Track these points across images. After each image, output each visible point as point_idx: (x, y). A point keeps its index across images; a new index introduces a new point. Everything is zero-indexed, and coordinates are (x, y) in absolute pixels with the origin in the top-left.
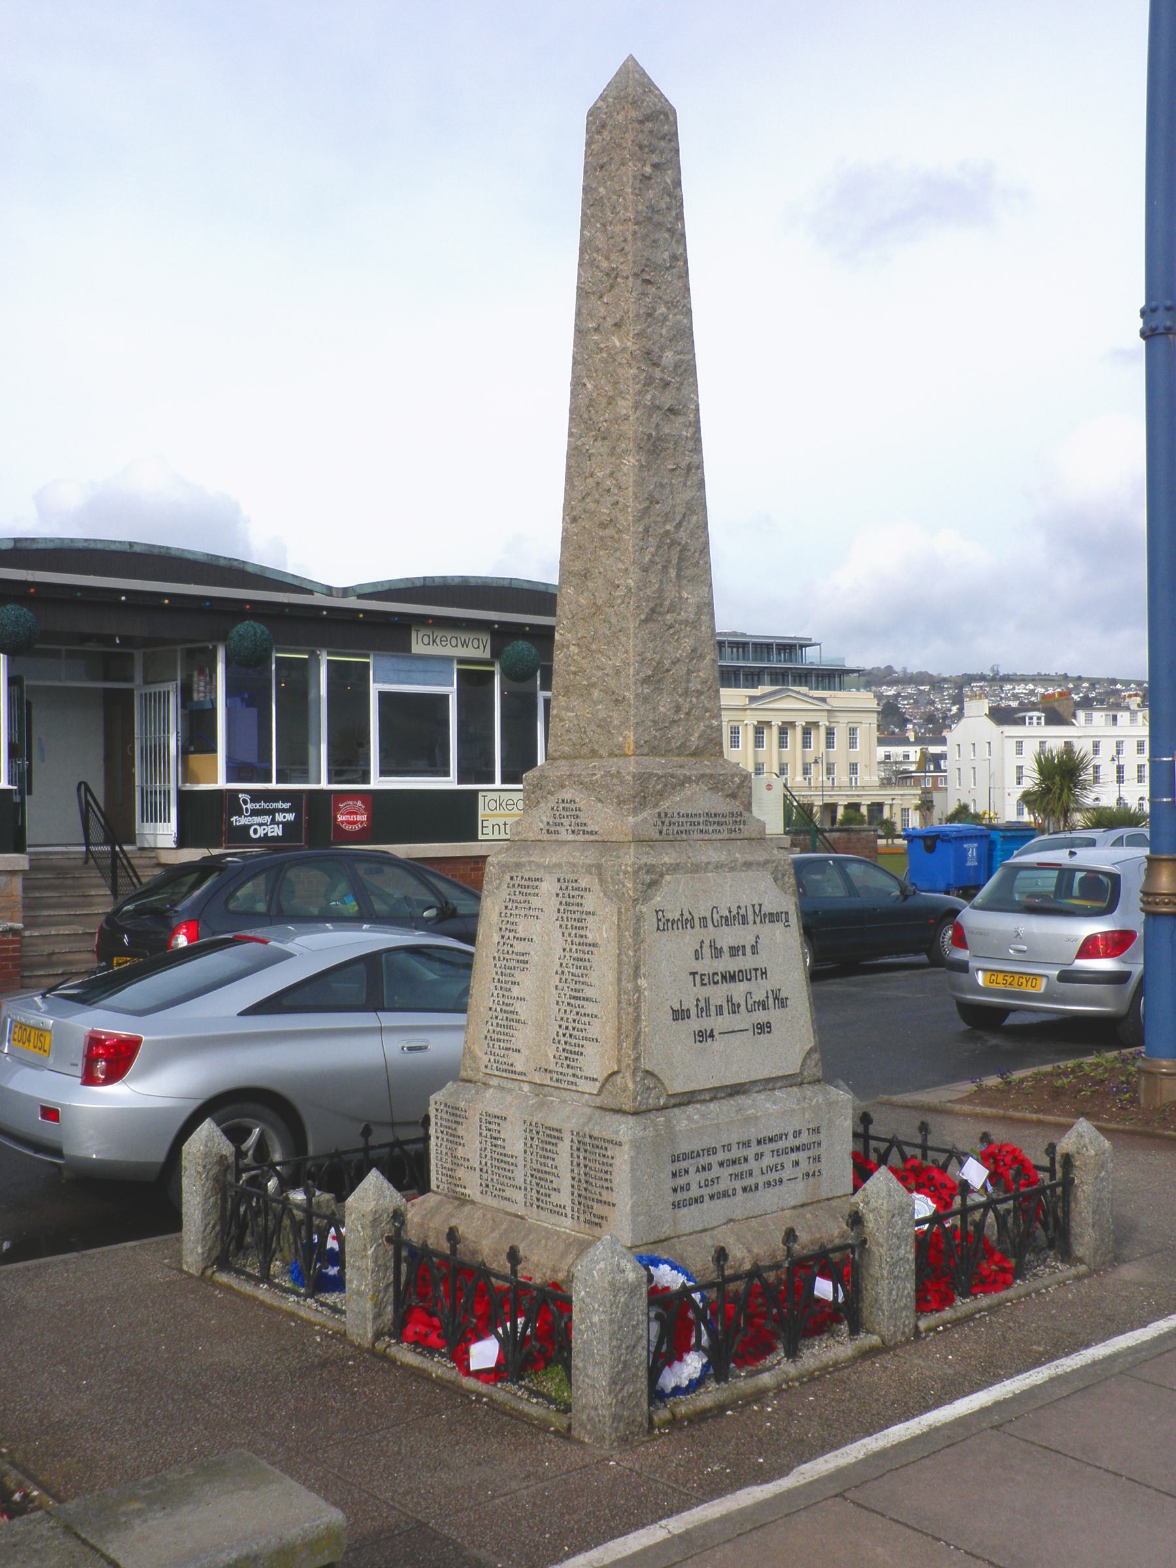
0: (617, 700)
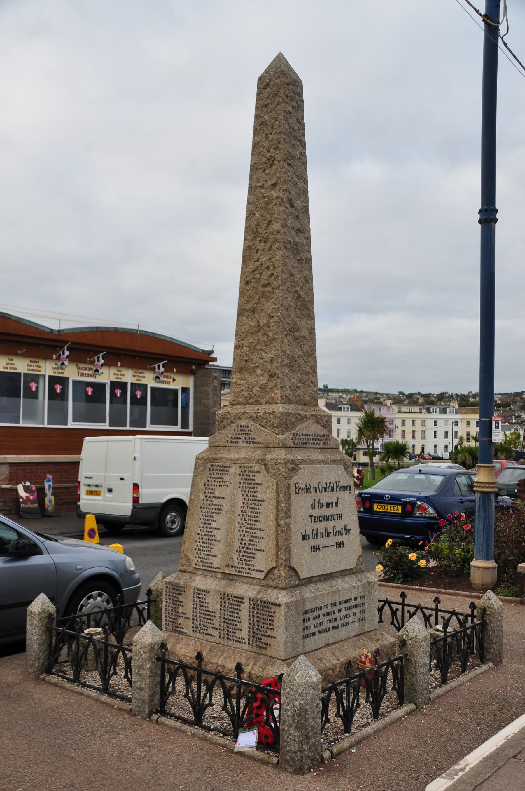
0: (271, 375)
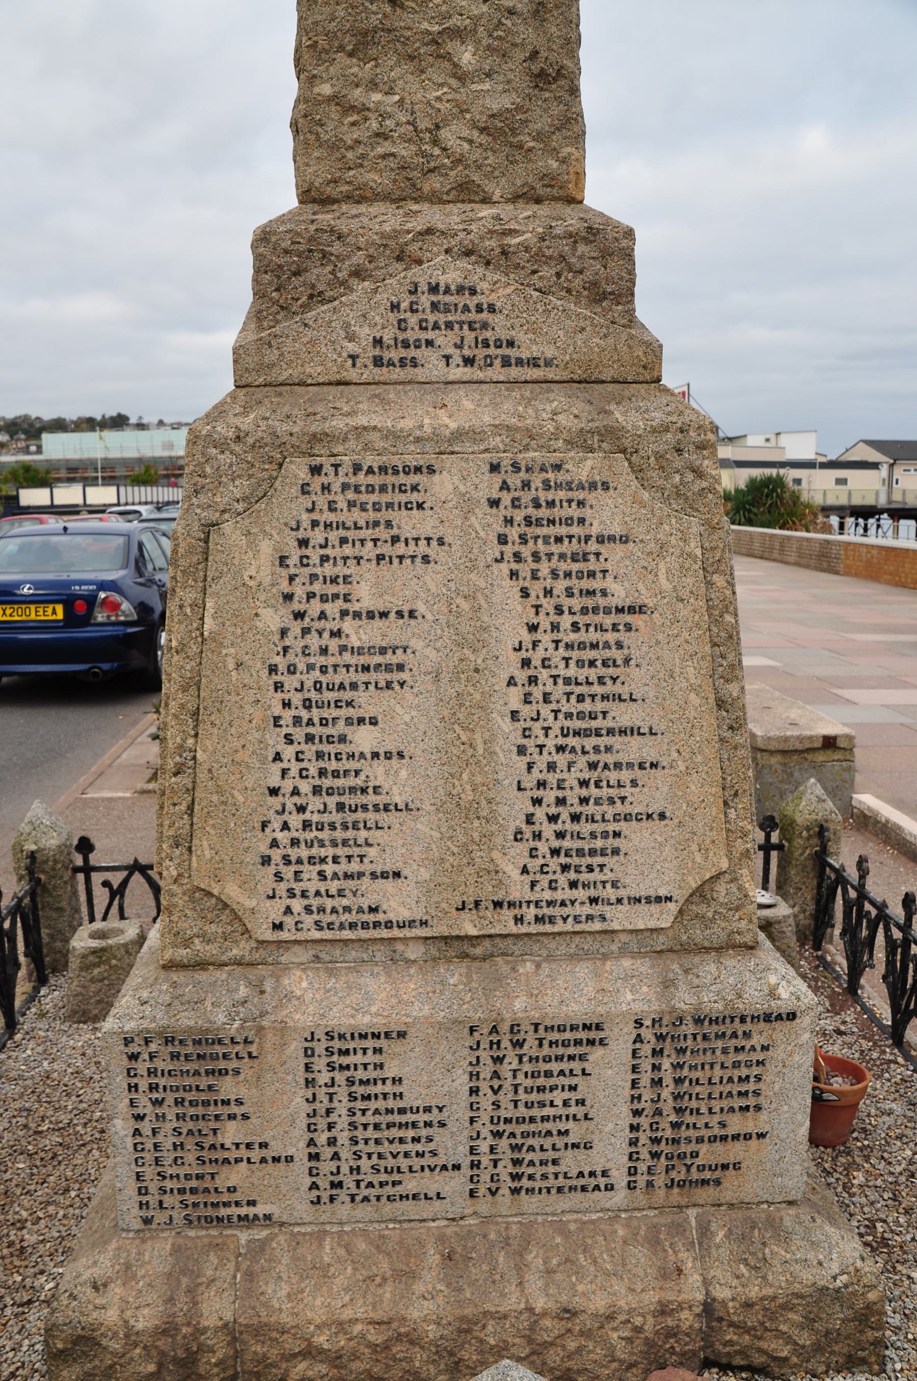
0: (542, 74)
